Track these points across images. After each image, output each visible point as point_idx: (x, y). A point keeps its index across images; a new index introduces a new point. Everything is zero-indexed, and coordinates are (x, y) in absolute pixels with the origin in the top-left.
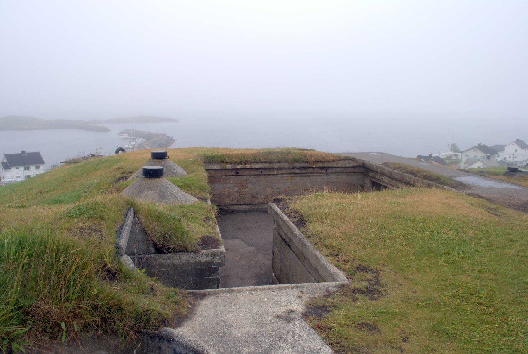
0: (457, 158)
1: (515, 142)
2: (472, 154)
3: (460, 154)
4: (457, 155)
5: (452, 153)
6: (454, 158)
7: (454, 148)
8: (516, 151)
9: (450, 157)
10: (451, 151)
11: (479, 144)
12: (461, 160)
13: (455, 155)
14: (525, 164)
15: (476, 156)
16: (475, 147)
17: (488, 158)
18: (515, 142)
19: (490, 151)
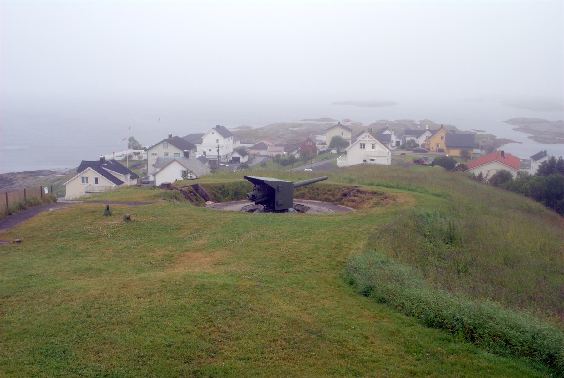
0: (140, 157)
1: (215, 129)
2: (161, 152)
3: (143, 151)
4: (139, 153)
5: (130, 151)
6: (136, 158)
7: (134, 144)
8: (217, 141)
9: (128, 158)
10: (129, 147)
11: (170, 136)
12: (146, 160)
13: (135, 153)
14: (231, 158)
15: (167, 154)
16: (165, 140)
17: (186, 155)
18: (215, 129)
19: (185, 145)
